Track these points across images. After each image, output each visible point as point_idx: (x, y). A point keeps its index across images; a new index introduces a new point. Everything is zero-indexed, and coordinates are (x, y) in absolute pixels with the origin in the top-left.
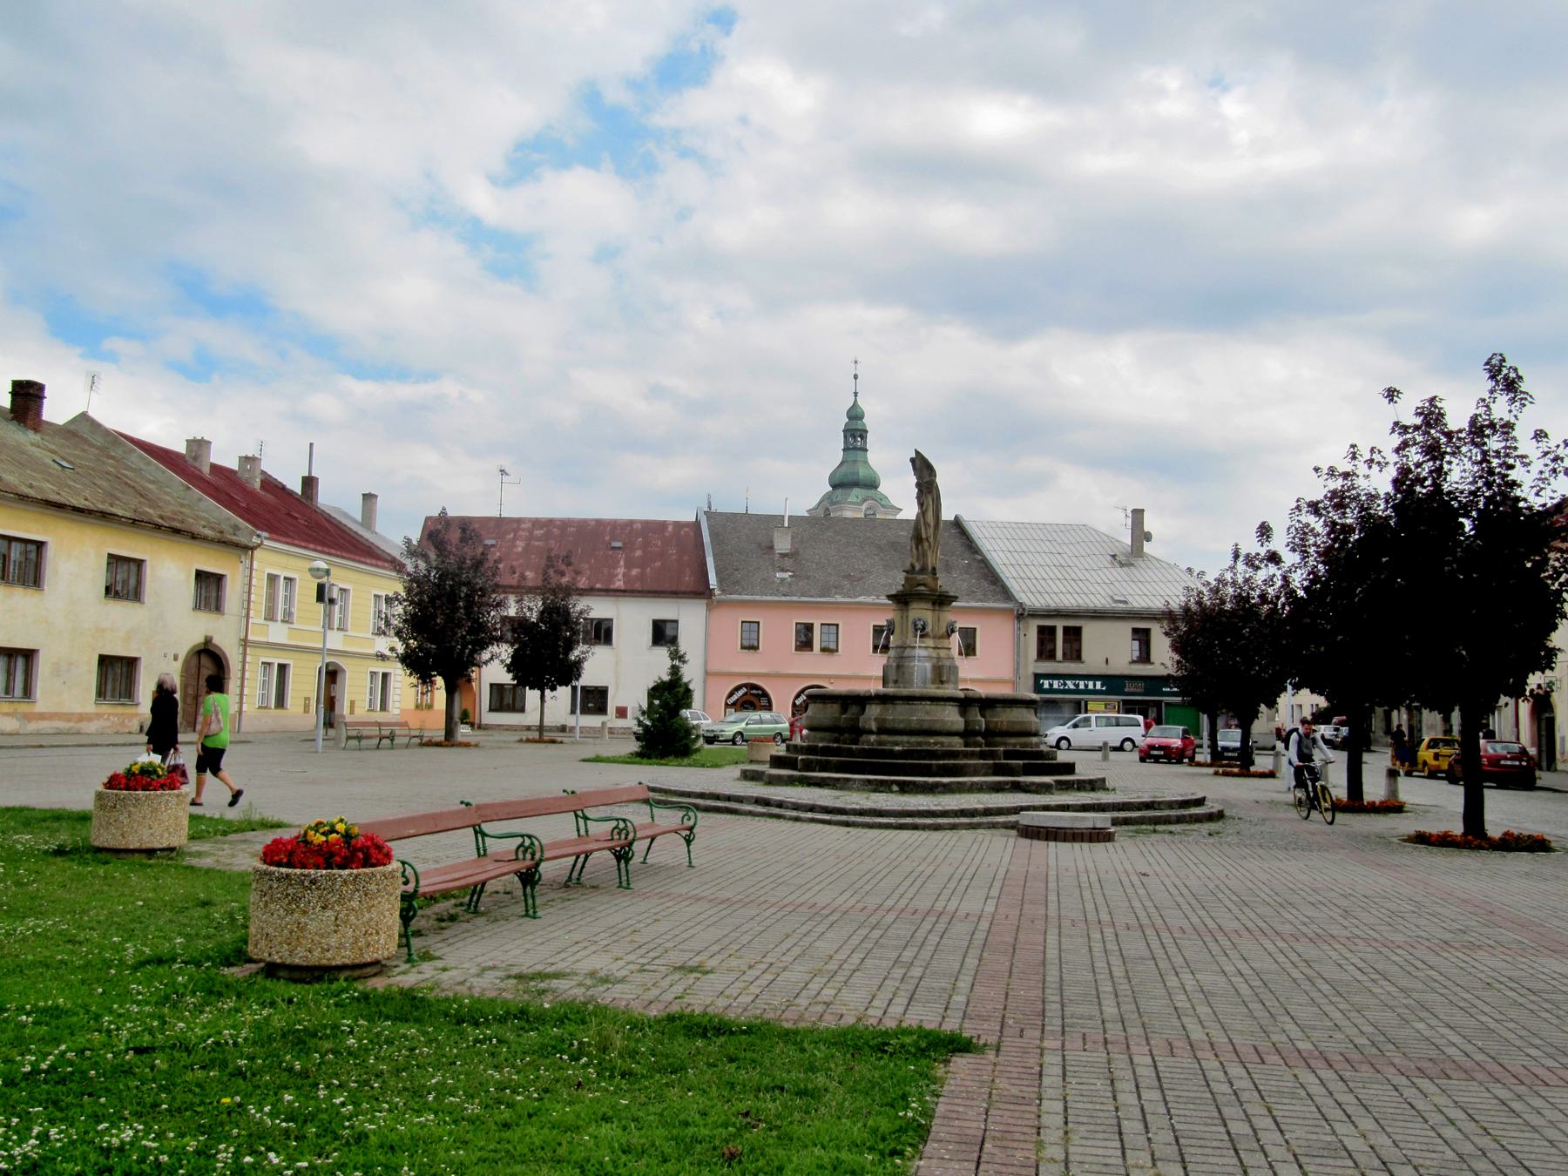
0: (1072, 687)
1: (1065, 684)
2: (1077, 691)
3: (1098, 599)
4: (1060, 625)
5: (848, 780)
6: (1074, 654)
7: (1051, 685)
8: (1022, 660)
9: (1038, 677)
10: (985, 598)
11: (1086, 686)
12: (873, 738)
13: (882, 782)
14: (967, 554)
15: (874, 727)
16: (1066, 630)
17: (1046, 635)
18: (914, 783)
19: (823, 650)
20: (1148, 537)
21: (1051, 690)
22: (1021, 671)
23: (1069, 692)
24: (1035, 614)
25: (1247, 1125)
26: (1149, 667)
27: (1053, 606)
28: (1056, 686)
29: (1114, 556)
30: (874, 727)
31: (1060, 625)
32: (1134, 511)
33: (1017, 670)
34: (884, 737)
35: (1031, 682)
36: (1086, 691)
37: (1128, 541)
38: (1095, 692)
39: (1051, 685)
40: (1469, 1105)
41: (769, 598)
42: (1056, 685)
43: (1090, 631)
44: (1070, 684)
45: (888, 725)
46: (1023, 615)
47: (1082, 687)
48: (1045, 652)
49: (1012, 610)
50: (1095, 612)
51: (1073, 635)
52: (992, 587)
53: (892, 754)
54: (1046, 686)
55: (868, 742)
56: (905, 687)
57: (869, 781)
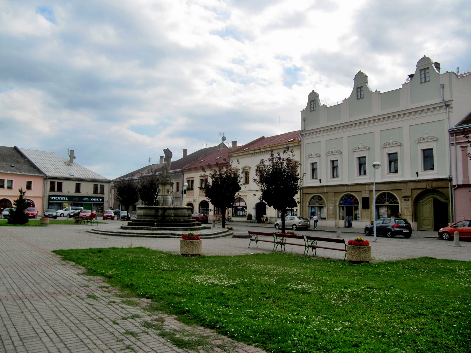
0: (59, 199)
1: (57, 198)
2: (61, 200)
3: (66, 175)
4: (56, 181)
5: (177, 228)
6: (60, 189)
7: (53, 198)
8: (45, 191)
9: (50, 196)
10: (29, 171)
11: (63, 199)
12: (172, 218)
13: (186, 228)
14: (22, 159)
15: (173, 215)
16: (58, 183)
17: (52, 184)
18: (193, 228)
19: (8, 188)
20: (74, 158)
21: (53, 200)
22: (45, 194)
23: (55, 200)
24: (50, 178)
25: (51, 330)
26: (62, 193)
27: (55, 176)
28: (64, 199)
29: (65, 162)
30: (173, 215)
31: (56, 181)
32: (71, 150)
33: (44, 194)
34: (176, 218)
35: (48, 197)
36: (63, 200)
37: (69, 159)
38: (65, 200)
39: (53, 198)
40: (62, 324)
41: (31, 174)
42: (55, 198)
43: (65, 183)
44: (59, 198)
45: (177, 215)
46: (46, 178)
47: (62, 199)
48: (52, 189)
49: (43, 177)
50: (66, 178)
51: (60, 185)
52: (35, 169)
53: (181, 222)
54: (52, 199)
55: (171, 219)
56: (166, 206)
57: (183, 228)
